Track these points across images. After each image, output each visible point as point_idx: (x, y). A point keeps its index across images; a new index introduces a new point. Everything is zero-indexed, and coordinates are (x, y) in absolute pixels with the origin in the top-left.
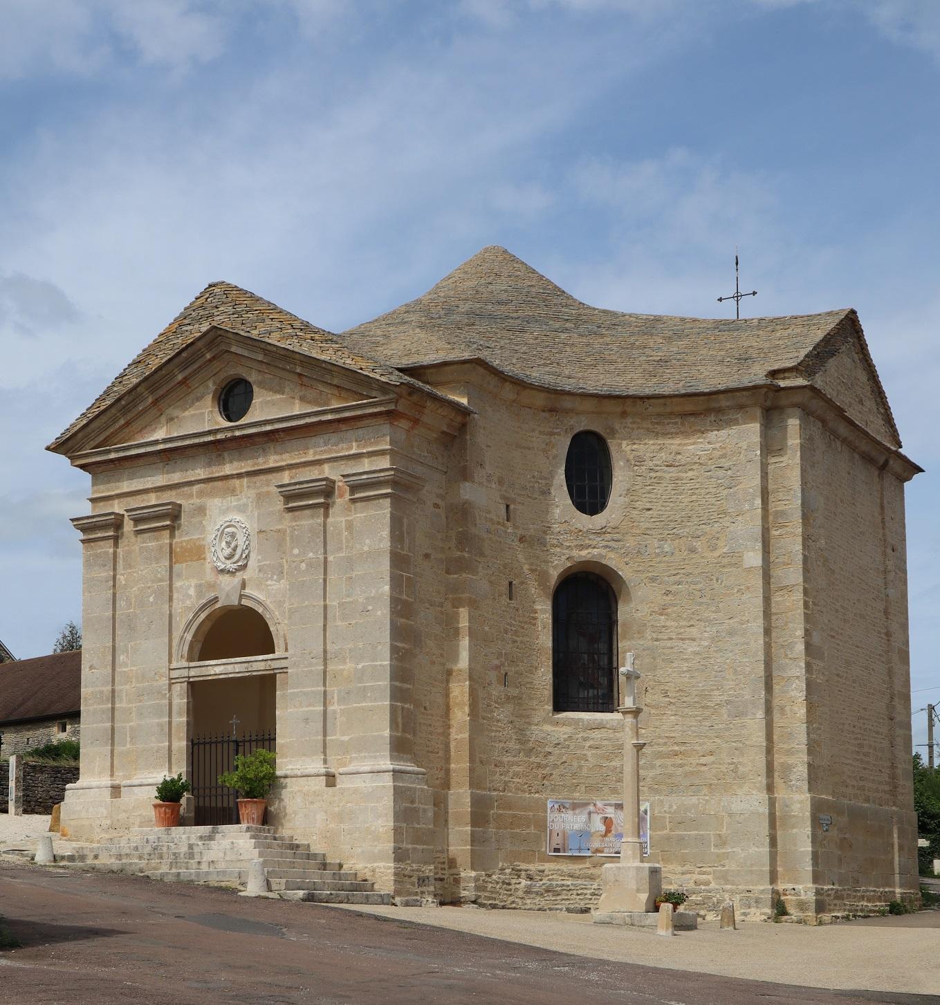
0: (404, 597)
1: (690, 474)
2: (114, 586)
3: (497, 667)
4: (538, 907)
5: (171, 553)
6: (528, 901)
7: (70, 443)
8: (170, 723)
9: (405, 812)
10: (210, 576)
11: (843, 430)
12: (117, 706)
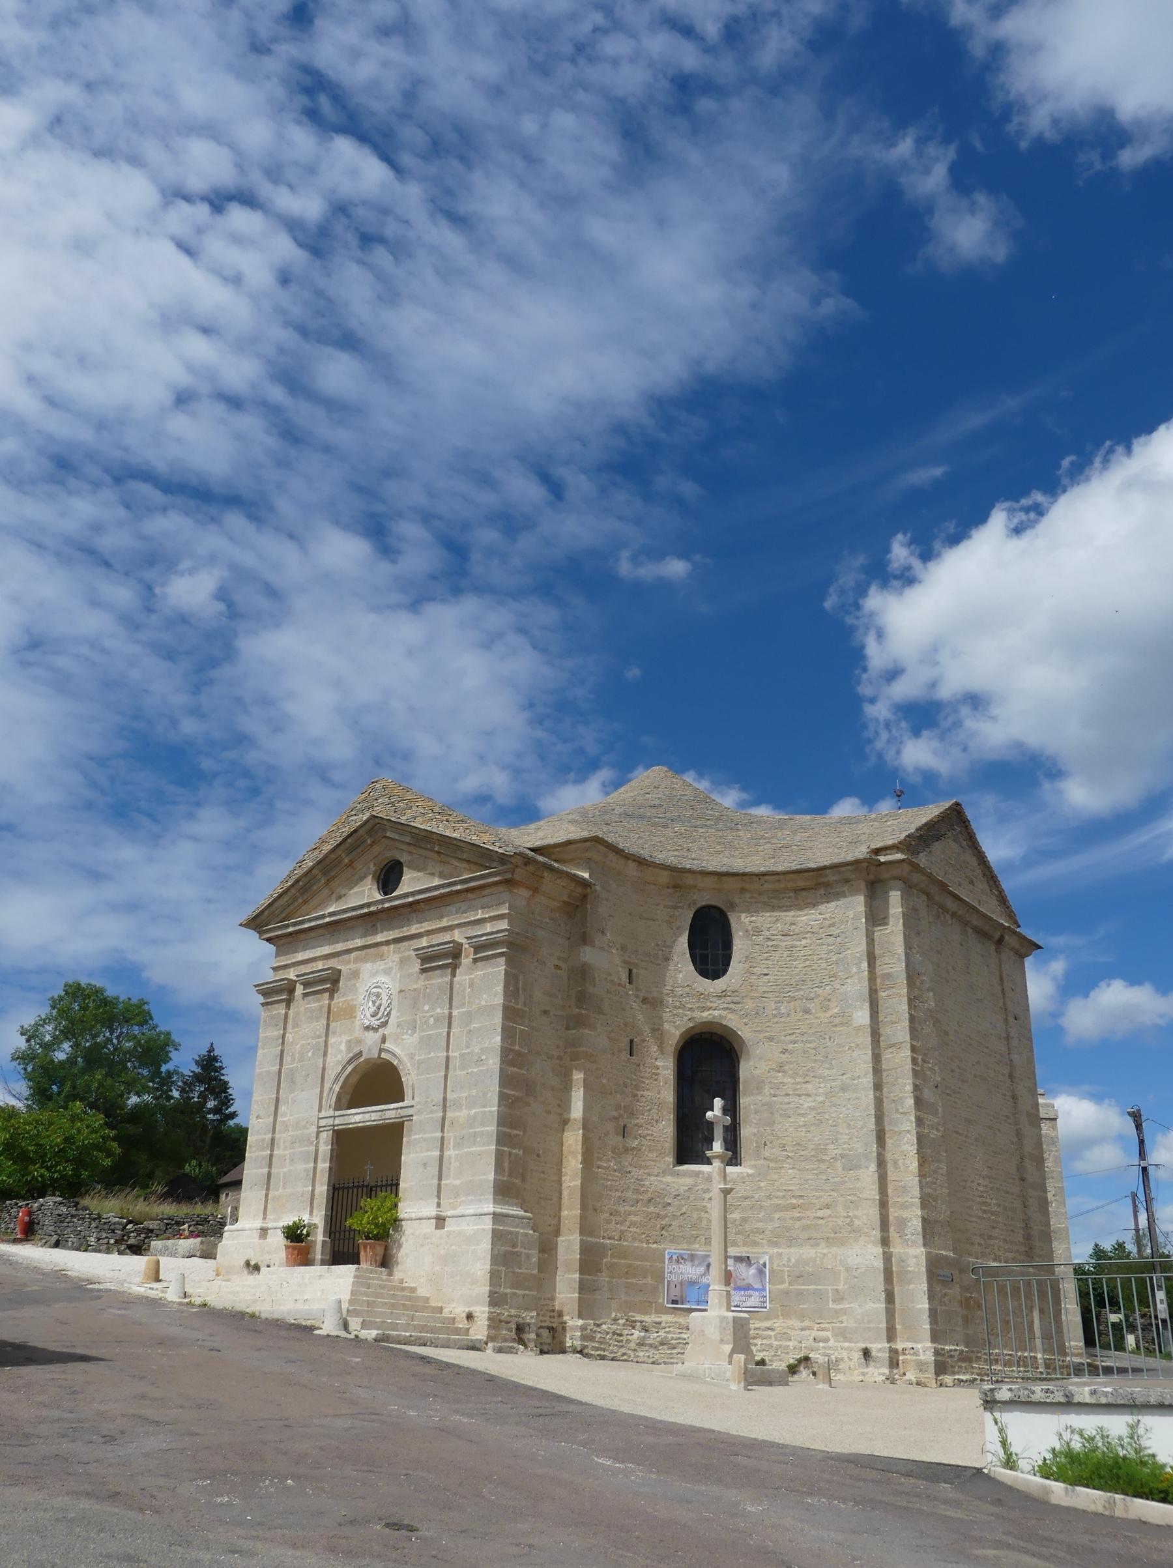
0: (517, 1048)
1: (804, 942)
2: (283, 1043)
3: (616, 1119)
4: (651, 1360)
5: (329, 1013)
6: (641, 1354)
7: (258, 921)
8: (315, 1168)
9: (505, 1255)
10: (358, 1032)
11: (950, 904)
12: (275, 1152)
